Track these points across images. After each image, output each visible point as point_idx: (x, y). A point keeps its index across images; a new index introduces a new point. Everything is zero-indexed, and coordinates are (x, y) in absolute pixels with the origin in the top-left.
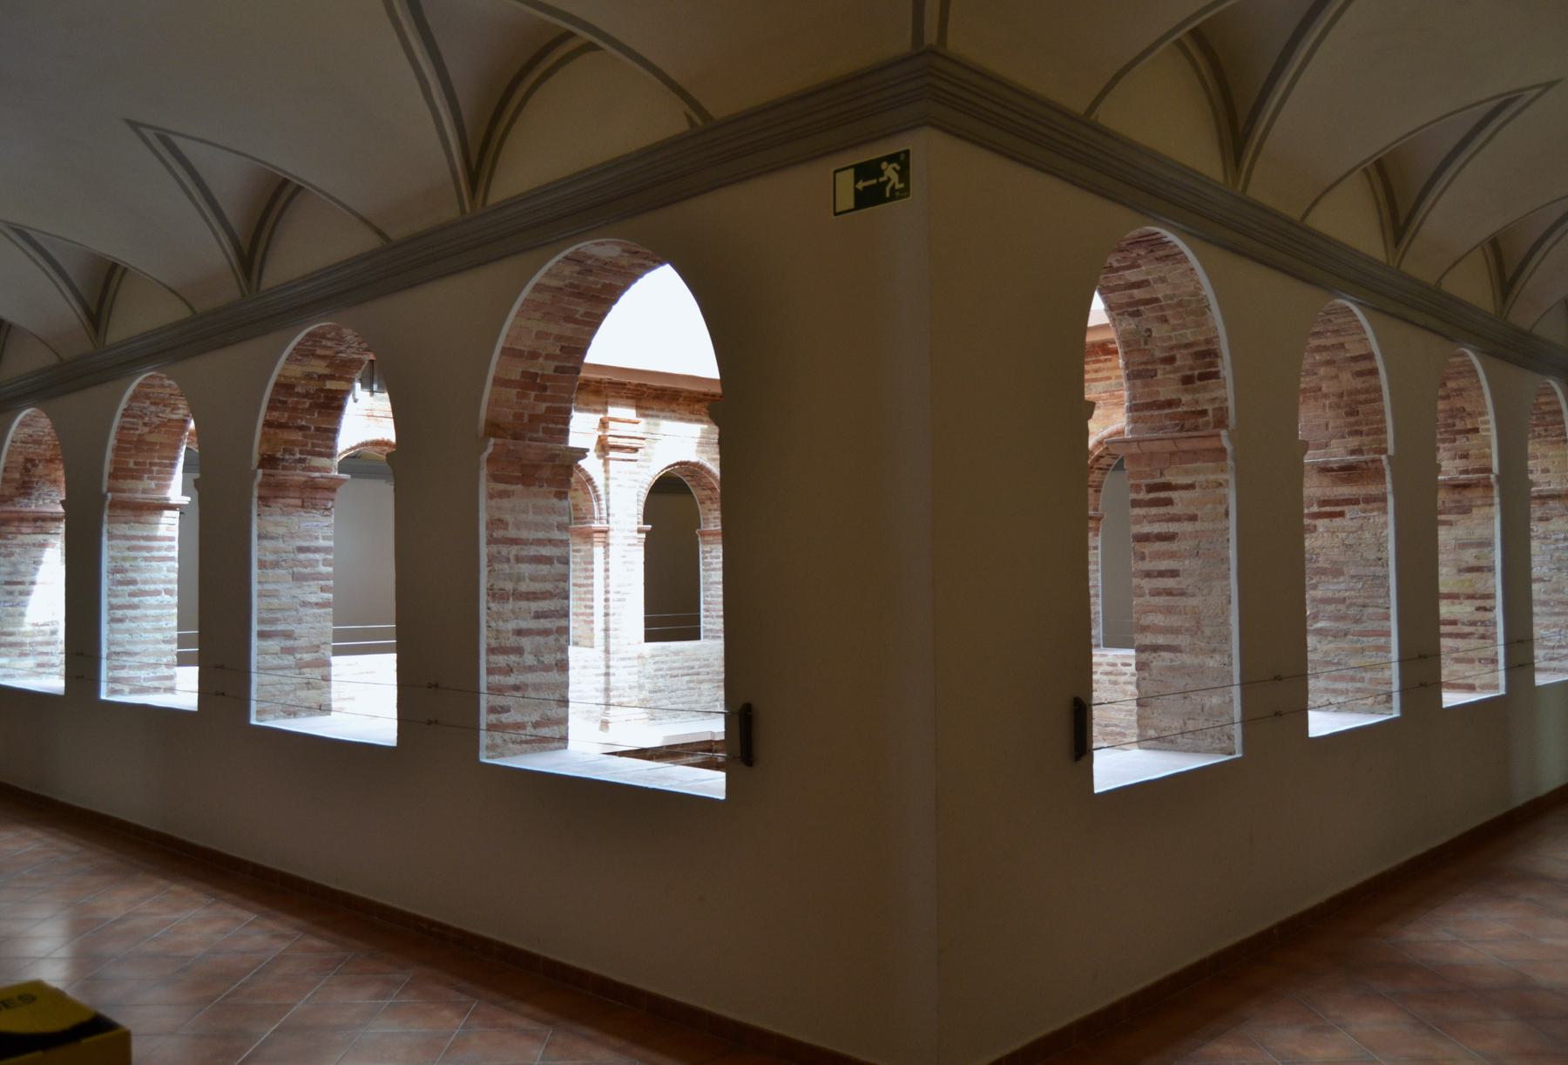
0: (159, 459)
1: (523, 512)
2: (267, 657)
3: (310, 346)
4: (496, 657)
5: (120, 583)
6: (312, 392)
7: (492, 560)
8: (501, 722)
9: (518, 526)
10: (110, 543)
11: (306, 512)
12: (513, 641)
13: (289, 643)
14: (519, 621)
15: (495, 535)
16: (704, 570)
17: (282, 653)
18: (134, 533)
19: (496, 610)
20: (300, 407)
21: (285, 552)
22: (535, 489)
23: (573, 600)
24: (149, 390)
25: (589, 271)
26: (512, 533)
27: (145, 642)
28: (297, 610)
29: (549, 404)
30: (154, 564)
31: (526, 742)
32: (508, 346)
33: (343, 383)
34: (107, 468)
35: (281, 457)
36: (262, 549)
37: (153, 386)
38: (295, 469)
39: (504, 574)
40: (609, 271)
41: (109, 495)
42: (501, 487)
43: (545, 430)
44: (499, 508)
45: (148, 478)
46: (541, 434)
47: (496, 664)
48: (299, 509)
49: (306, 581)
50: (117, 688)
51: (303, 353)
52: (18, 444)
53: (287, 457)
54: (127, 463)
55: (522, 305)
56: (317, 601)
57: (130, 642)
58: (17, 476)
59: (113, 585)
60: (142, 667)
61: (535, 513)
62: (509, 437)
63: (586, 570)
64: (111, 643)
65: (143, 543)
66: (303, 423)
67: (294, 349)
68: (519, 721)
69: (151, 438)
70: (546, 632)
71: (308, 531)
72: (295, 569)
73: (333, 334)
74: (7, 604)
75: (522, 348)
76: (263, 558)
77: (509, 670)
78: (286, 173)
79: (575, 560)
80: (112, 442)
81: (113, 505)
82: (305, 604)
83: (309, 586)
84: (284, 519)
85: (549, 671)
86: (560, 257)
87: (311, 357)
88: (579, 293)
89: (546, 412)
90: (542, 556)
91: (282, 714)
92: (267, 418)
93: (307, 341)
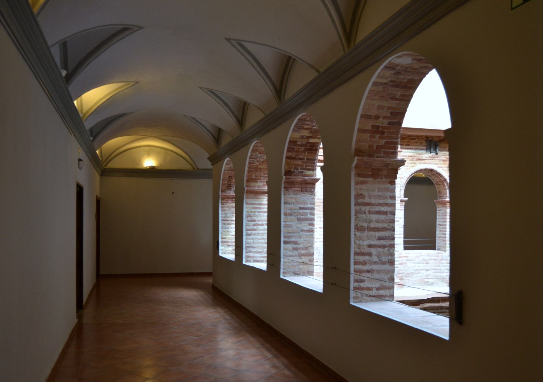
0: (263, 174)
1: (373, 191)
2: (287, 251)
3: (300, 124)
4: (358, 257)
5: (250, 221)
6: (304, 144)
7: (357, 212)
8: (360, 286)
9: (370, 197)
10: (247, 206)
11: (303, 193)
12: (367, 250)
13: (296, 246)
14: (370, 241)
15: (359, 201)
16: (221, 210)
17: (293, 250)
18: (254, 202)
19: (359, 235)
20: (300, 150)
21: (294, 209)
22: (378, 180)
23: (438, 231)
24: (257, 148)
25: (399, 73)
26: (367, 200)
27: (258, 243)
28: (299, 233)
29: (386, 140)
30: (262, 214)
31: (373, 296)
32: (364, 113)
33: (316, 139)
34: (245, 178)
35: (293, 171)
36: (285, 208)
37: (258, 147)
38: (299, 176)
39: (363, 219)
40: (409, 72)
41: (246, 188)
42: (362, 179)
43: (385, 153)
44: (361, 189)
45: (260, 182)
46: (382, 154)
47: (358, 260)
48: (300, 192)
49: (303, 221)
50: (249, 260)
51: (299, 127)
52: (226, 171)
53: (296, 171)
54: (252, 176)
55: (368, 93)
56: (307, 229)
57: (253, 243)
58: (227, 182)
59: (247, 221)
60: (257, 252)
61: (378, 191)
62: (366, 156)
63: (443, 219)
64: (247, 243)
65: (258, 206)
66: (302, 157)
67: (295, 126)
68: (369, 287)
69: (260, 167)
70: (384, 246)
71: (303, 201)
72: (298, 216)
73: (309, 118)
74: (223, 228)
75: (371, 114)
76: (285, 212)
77: (364, 263)
78: (290, 54)
79: (439, 214)
80: (247, 168)
81: (247, 192)
82: (302, 230)
83: (304, 223)
84: (294, 196)
85: (384, 264)
86: (382, 67)
87: (302, 129)
88: (397, 85)
89: (385, 144)
90: (382, 211)
91: (293, 274)
92: (287, 155)
93: (299, 122)
